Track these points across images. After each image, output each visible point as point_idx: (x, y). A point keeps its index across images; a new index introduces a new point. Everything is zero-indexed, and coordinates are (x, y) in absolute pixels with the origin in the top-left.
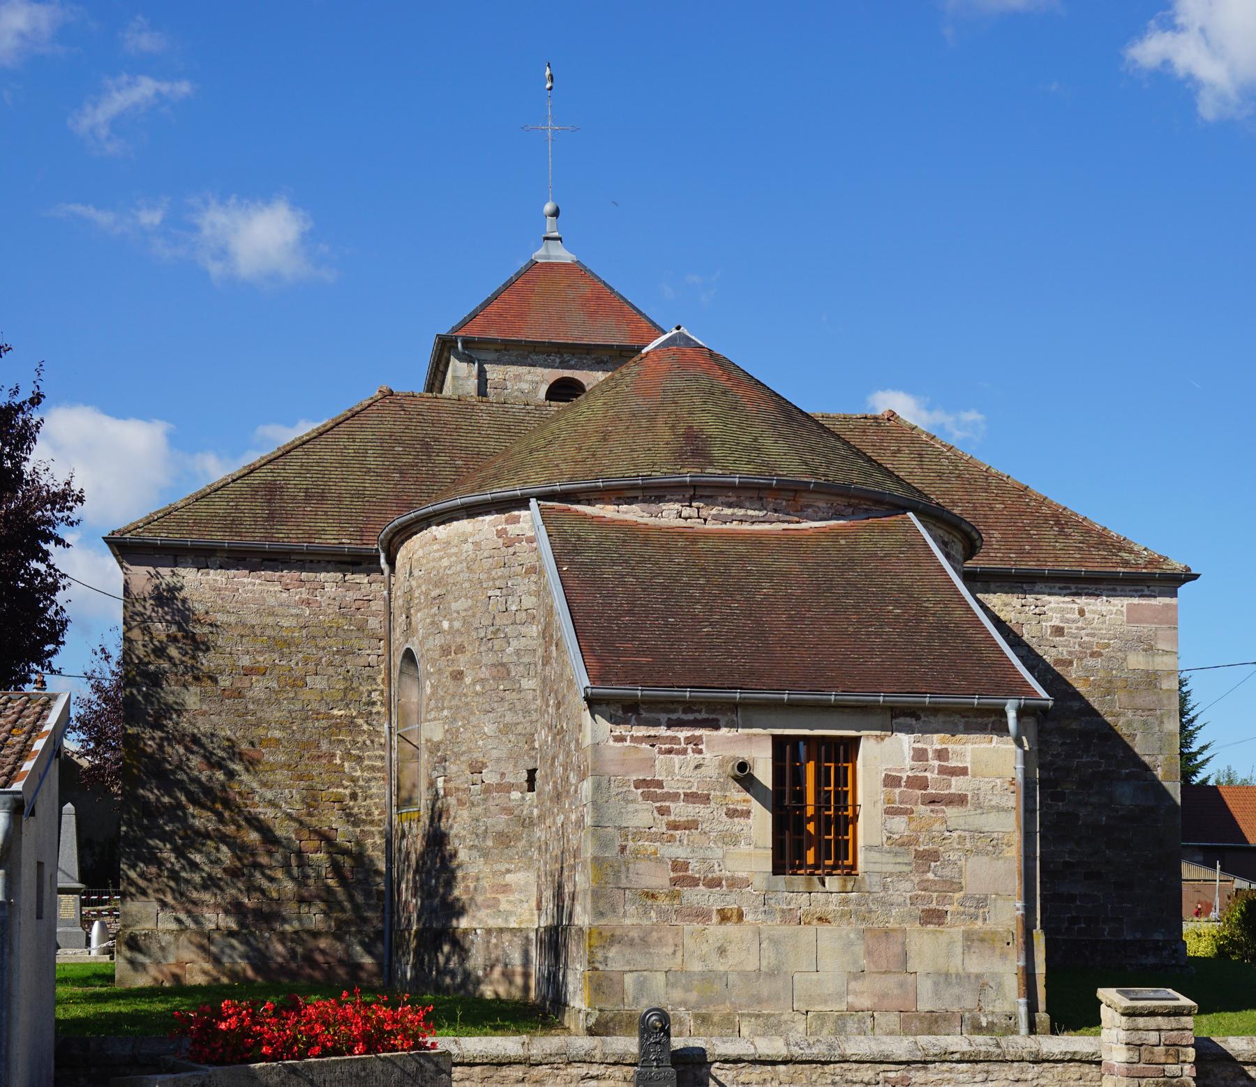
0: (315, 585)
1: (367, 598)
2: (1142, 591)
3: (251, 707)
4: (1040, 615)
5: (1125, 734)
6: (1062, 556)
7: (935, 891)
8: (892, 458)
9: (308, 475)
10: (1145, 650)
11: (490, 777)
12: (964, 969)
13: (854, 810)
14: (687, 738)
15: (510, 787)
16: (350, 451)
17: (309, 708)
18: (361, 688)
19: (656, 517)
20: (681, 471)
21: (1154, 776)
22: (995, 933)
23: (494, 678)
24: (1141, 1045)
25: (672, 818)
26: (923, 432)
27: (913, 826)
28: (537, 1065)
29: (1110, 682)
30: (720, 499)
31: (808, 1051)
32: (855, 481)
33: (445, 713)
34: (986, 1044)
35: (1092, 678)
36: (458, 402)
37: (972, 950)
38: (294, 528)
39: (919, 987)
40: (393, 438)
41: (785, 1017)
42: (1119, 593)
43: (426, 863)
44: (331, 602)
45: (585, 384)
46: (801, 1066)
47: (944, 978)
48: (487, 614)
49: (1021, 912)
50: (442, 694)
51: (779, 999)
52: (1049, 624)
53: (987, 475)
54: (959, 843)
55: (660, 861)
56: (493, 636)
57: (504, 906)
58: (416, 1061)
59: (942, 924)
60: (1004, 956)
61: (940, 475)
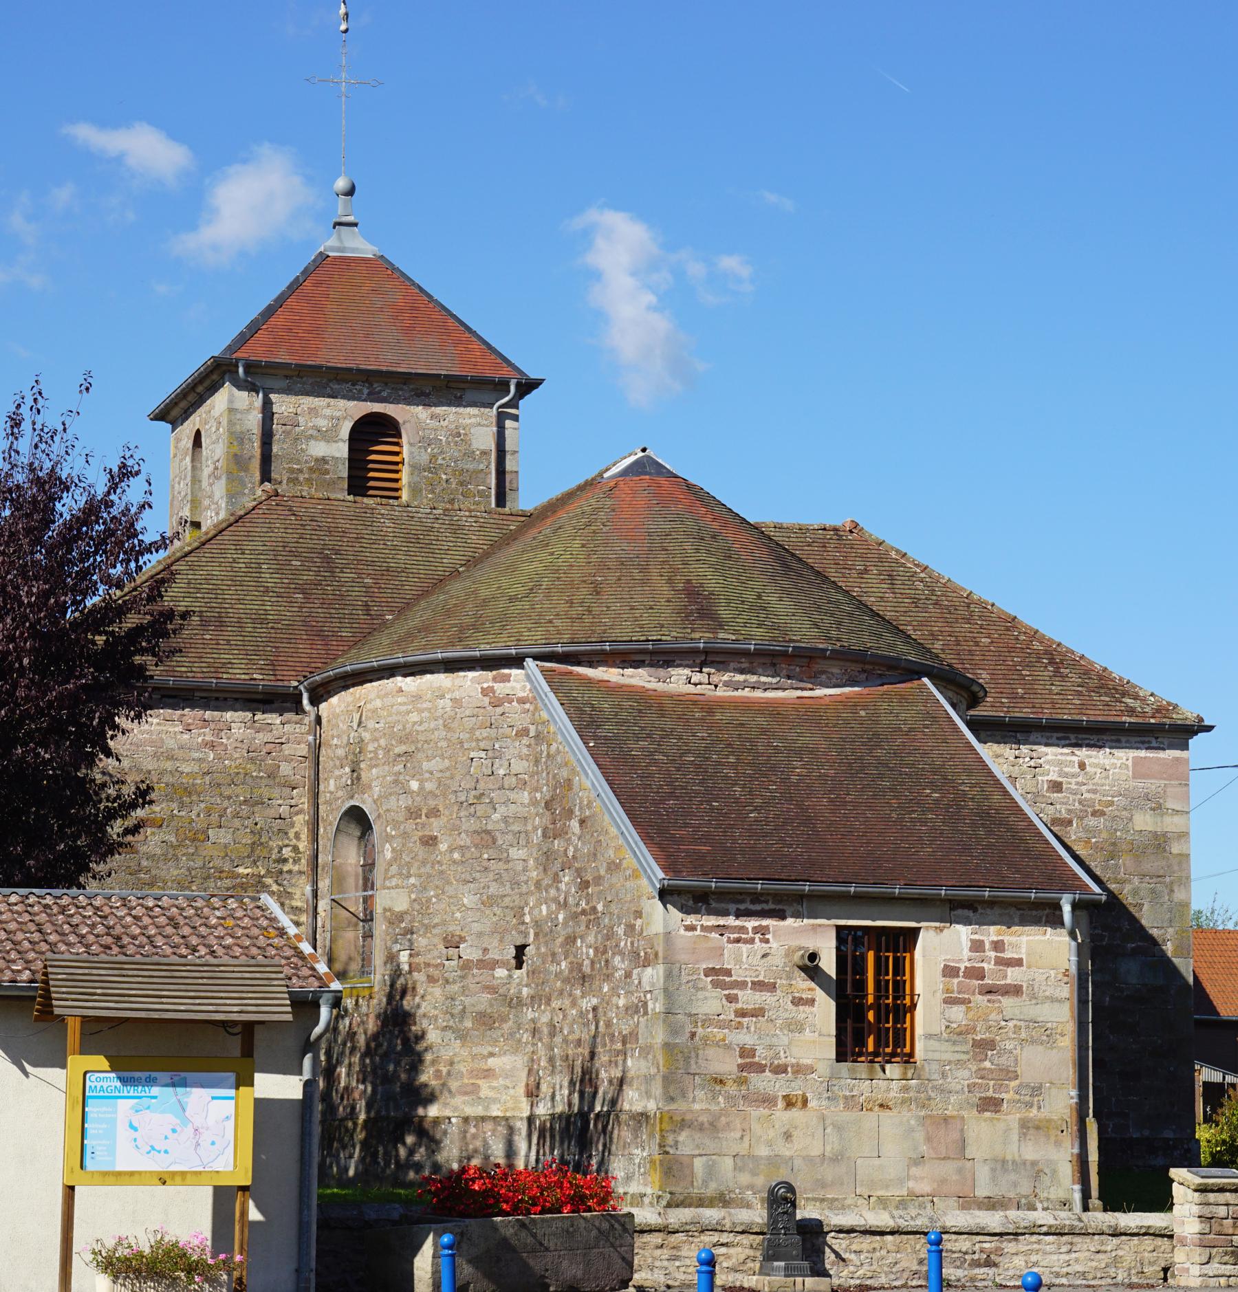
0: (221, 726)
1: (279, 741)
2: (1149, 742)
3: (144, 863)
4: (1035, 768)
5: (1130, 904)
6: (1060, 701)
7: (992, 1079)
8: (858, 580)
9: (198, 595)
10: (1152, 809)
11: (469, 952)
12: (1020, 1156)
13: (912, 999)
14: (754, 928)
15: (494, 964)
16: (241, 565)
17: (211, 865)
18: (271, 843)
19: (664, 682)
20: (693, 636)
21: (1162, 951)
22: (1049, 1121)
23: (476, 846)
24: (1212, 1218)
25: (739, 1006)
26: (892, 548)
27: (970, 1015)
28: (674, 1233)
29: (1114, 844)
30: (732, 665)
31: (912, 1223)
32: (869, 645)
33: (412, 880)
34: (1070, 1219)
35: (1094, 840)
36: (354, 505)
37: (1028, 1138)
38: (197, 660)
39: (977, 1173)
40: (287, 549)
41: (848, 1202)
42: (1124, 745)
43: (381, 1045)
44: (239, 745)
45: (401, 421)
46: (906, 1237)
47: (1001, 1165)
48: (468, 777)
49: (1075, 1100)
50: (407, 860)
51: (842, 1184)
52: (1046, 778)
53: (969, 601)
54: (1014, 1033)
55: (728, 1047)
56: (475, 801)
57: (485, 1092)
58: (608, 1221)
59: (999, 1111)
60: (1058, 1143)
61: (915, 602)
